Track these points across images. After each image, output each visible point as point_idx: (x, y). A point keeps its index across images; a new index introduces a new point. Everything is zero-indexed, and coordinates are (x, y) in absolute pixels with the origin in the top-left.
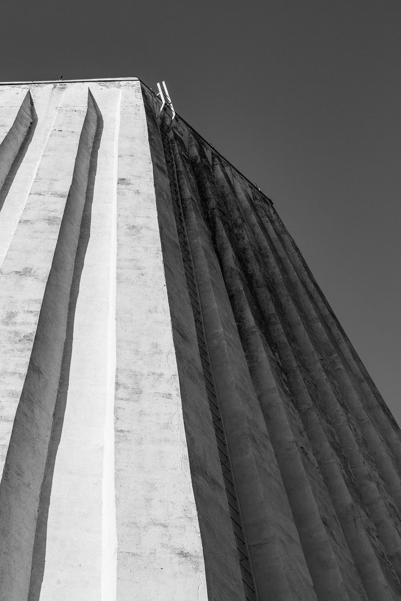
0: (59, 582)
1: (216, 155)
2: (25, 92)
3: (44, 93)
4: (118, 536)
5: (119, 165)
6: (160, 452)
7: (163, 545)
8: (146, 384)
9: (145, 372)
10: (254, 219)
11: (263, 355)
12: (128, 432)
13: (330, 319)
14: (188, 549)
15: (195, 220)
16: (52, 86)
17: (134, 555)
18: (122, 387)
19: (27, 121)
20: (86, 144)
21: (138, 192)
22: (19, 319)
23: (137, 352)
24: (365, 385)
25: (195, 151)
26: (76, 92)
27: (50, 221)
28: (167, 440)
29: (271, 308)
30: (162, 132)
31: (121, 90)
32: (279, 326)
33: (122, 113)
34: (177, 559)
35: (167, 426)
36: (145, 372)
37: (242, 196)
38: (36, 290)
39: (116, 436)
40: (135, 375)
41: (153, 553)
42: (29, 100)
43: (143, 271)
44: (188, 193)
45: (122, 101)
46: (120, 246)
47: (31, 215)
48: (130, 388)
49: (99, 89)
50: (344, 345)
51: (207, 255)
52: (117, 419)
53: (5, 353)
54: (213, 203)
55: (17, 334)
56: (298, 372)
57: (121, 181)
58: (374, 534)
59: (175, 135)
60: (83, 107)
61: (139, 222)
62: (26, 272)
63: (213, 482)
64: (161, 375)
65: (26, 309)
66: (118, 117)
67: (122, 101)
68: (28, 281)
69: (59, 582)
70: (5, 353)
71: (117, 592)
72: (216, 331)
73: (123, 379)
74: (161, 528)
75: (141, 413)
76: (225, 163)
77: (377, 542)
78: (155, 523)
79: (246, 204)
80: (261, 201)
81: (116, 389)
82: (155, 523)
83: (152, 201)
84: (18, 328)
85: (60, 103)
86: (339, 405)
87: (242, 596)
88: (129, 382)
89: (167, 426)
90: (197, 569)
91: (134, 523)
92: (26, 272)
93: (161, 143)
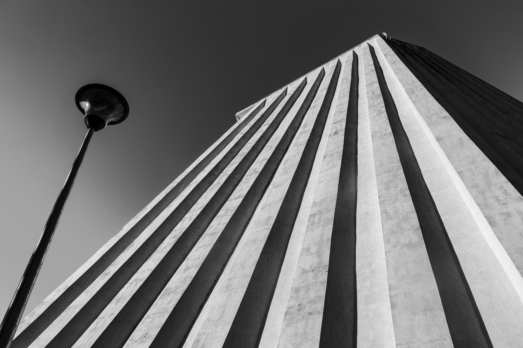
3: (357, 49)
5: (414, 102)
8: (415, 90)
10: (422, 52)
11: (440, 77)
14: (445, 116)
15: (407, 55)
19: (355, 57)
22: (376, 92)
25: (399, 44)
27: (372, 71)
29: (437, 68)
30: (390, 42)
33: (378, 43)
35: (425, 95)
38: (377, 85)
40: (411, 89)
41: (436, 120)
42: (354, 52)
44: (403, 51)
45: (376, 41)
46: (392, 67)
47: (367, 72)
48: (410, 92)
49: (369, 41)
54: (410, 52)
57: (385, 55)
60: (368, 46)
61: (394, 60)
62: (372, 83)
66: (377, 44)
67: (376, 41)
68: (374, 85)
73: (408, 91)
78: (433, 115)
79: (418, 50)
80: (422, 49)
82: (433, 115)
85: (361, 50)
88: (410, 91)
89: (425, 95)
92: (372, 83)
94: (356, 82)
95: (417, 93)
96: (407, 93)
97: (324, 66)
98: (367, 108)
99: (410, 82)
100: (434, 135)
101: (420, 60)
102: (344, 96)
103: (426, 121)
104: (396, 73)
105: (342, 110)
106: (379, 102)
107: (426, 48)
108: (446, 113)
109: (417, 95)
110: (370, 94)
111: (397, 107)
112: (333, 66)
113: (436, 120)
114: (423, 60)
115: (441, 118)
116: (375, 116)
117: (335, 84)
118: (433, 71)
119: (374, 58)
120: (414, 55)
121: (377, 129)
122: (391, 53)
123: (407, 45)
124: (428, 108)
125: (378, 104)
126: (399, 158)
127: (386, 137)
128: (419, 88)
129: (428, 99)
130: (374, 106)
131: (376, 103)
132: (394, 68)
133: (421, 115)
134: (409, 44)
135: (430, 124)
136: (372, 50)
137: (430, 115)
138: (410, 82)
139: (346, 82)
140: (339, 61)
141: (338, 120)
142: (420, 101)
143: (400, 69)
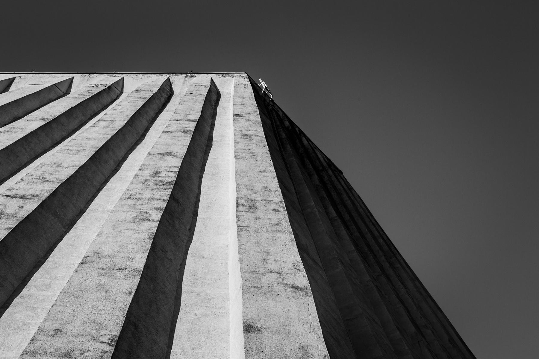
0: (196, 315)
2: (166, 78)
4: (242, 278)
5: (241, 228)
9: (259, 199)
11: (343, 232)
12: (247, 226)
14: (298, 284)
16: (185, 75)
17: (255, 287)
18: (241, 224)
20: (210, 102)
22: (163, 174)
24: (417, 283)
25: (287, 123)
26: (203, 80)
28: (277, 231)
29: (347, 217)
31: (234, 79)
34: (290, 289)
36: (259, 199)
39: (238, 229)
43: (255, 154)
46: (236, 143)
48: (246, 206)
49: (218, 80)
52: (239, 220)
53: (152, 190)
55: (161, 181)
61: (250, 133)
64: (271, 201)
65: (168, 170)
67: (235, 89)
68: (169, 158)
69: (196, 315)
70: (152, 190)
71: (243, 306)
72: (309, 204)
73: (241, 202)
78: (271, 272)
81: (237, 207)
82: (271, 272)
83: (259, 124)
84: (161, 179)
85: (190, 89)
86: (399, 282)
90: (306, 295)
91: (255, 271)
94: (131, 140)
95: (259, 214)
96: (238, 205)
97: (78, 78)
98: (119, 195)
99: (258, 187)
100: (244, 316)
101: (316, 177)
102: (79, 152)
103: (244, 279)
104: (236, 157)
105: (48, 177)
106: (157, 197)
107: (346, 175)
108: (302, 280)
109: (257, 218)
110: (146, 173)
111: (197, 229)
112: (98, 86)
113: (271, 286)
114: (321, 179)
115: (287, 285)
116: (125, 221)
117: (76, 123)
118: (333, 213)
119: (209, 112)
120: (307, 162)
121: (107, 250)
122: (252, 118)
123: (304, 139)
124: (268, 254)
125: (152, 199)
126: (83, 163)
127: (119, 274)
128: (273, 206)
129: (278, 235)
130: (138, 199)
131: (147, 195)
132: (241, 146)
133: (241, 260)
134: (308, 140)
135: (250, 289)
136: (213, 98)
137: (262, 270)
138: (258, 187)
139: (105, 127)
140: (120, 84)
141: (21, 193)
142: (257, 231)
143: (253, 154)
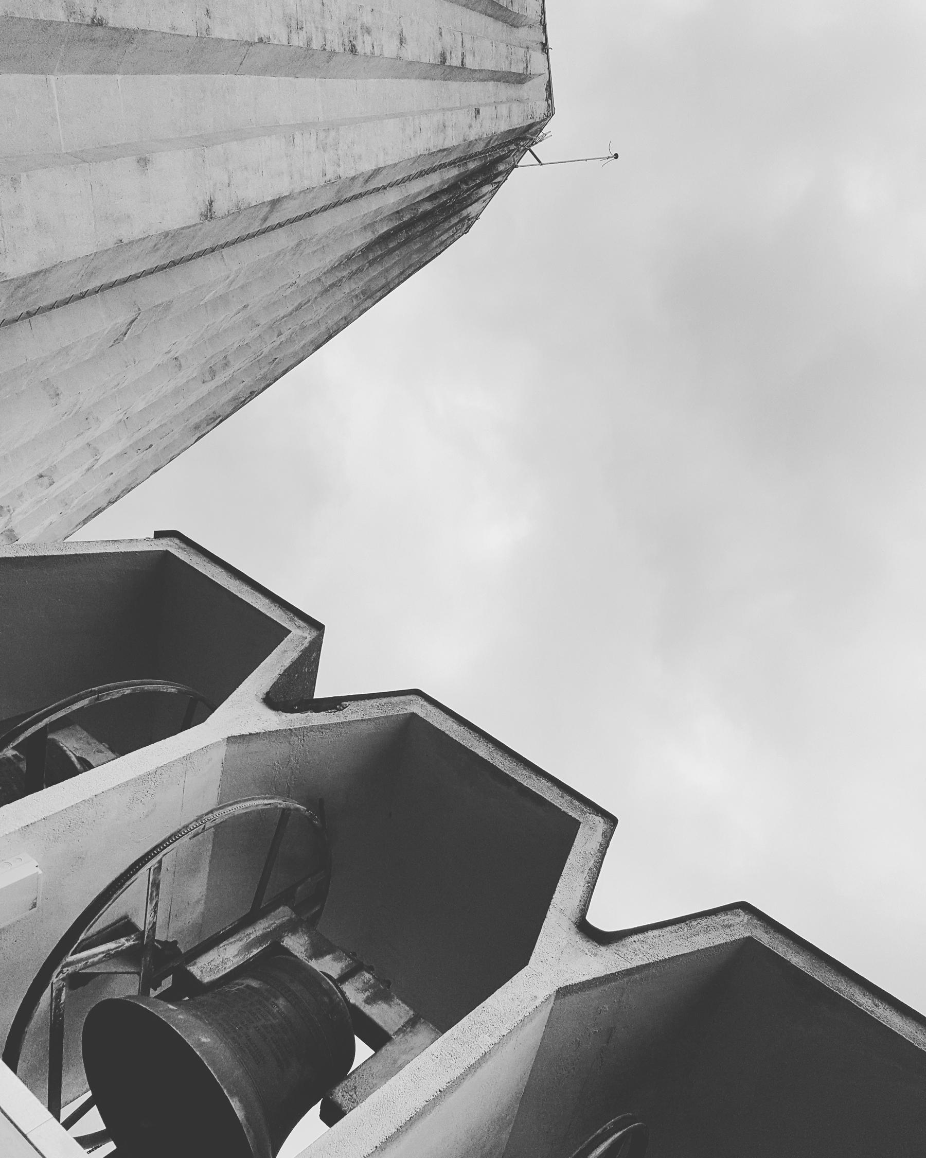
1: (499, 185)
6: (282, 173)
7: (215, 185)
13: (388, 289)
21: (470, 127)
22: (367, 38)
23: (353, 143)
32: (380, 252)
34: (207, 198)
37: (470, 209)
50: (369, 302)
51: (427, 189)
55: (355, 38)
56: (348, 271)
58: (241, 344)
59: (513, 150)
63: (265, 219)
64: (339, 165)
74: (227, 182)
75: (309, 153)
76: (493, 193)
77: (236, 345)
84: (360, 38)
87: (1, 927)
93: (404, 206)
